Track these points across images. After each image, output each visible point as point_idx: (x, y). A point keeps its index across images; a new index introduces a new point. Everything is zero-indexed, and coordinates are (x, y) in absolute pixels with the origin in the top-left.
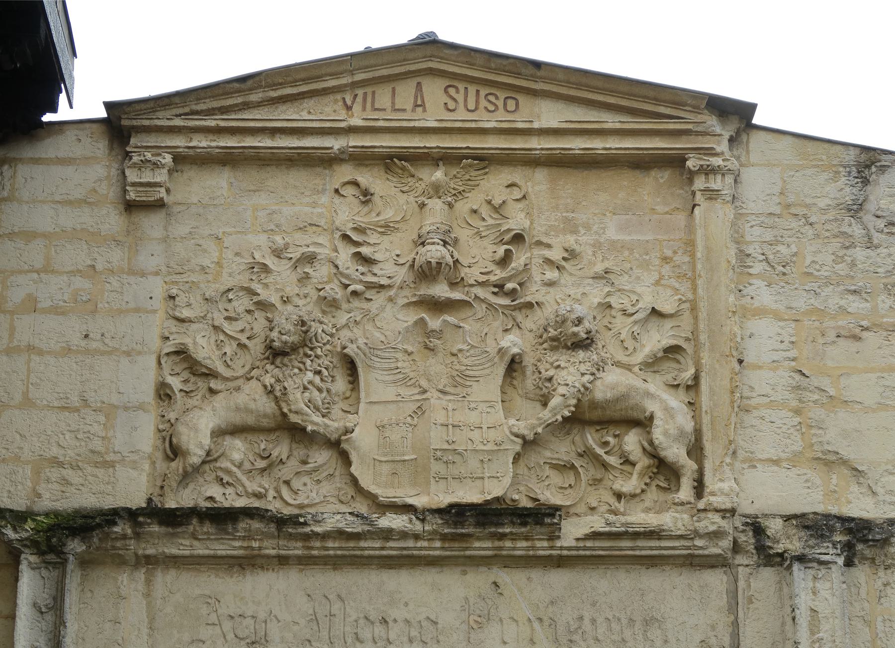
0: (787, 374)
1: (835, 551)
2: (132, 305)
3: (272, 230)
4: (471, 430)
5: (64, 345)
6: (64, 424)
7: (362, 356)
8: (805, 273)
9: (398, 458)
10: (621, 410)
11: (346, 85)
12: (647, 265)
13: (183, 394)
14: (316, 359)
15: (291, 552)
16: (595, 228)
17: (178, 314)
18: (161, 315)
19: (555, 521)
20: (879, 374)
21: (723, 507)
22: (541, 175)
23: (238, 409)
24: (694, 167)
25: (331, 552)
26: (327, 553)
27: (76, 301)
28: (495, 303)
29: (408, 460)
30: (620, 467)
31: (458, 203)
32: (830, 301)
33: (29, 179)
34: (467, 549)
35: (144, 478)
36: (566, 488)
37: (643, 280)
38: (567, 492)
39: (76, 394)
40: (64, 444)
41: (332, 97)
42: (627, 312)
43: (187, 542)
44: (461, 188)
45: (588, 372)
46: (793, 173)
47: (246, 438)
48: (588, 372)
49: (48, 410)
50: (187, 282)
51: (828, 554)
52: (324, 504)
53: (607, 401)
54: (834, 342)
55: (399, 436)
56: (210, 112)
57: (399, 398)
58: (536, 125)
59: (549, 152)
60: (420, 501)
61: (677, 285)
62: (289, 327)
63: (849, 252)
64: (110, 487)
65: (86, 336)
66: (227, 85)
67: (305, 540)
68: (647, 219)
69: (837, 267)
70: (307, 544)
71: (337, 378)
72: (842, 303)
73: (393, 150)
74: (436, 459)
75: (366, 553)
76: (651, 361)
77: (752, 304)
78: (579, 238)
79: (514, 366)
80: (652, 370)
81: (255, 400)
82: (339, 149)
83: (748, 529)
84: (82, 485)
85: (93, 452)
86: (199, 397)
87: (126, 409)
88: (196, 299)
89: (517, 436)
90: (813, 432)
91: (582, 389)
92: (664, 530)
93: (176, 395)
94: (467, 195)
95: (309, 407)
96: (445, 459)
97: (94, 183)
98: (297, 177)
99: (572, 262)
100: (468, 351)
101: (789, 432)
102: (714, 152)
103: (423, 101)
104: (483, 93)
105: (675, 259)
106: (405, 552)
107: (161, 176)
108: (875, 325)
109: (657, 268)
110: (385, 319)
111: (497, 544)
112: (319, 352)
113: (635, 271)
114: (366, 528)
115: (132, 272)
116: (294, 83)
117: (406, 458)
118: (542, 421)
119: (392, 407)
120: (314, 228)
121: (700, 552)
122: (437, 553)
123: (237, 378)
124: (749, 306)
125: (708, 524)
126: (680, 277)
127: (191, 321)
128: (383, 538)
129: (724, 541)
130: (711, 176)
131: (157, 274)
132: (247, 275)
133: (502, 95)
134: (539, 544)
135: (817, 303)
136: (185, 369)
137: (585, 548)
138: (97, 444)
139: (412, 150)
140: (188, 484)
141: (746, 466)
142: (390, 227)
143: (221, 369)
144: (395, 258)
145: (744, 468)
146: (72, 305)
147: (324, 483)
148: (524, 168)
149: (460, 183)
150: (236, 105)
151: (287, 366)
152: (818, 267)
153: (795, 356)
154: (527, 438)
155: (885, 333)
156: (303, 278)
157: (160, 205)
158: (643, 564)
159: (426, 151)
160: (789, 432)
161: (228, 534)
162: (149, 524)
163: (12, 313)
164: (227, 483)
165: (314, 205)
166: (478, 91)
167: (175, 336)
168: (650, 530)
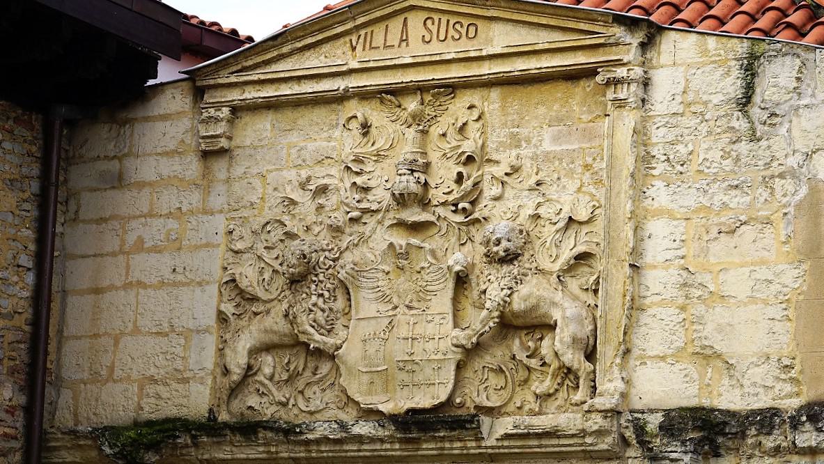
0: (677, 272)
1: (683, 449)
2: (204, 241)
3: (300, 165)
4: (427, 341)
5: (160, 279)
6: (159, 347)
7: (351, 279)
8: (698, 171)
9: (374, 369)
10: (536, 317)
11: (351, 29)
12: (572, 173)
13: (236, 316)
14: (319, 283)
15: (298, 455)
16: (534, 141)
17: (233, 247)
18: (223, 248)
19: (474, 426)
20: (752, 268)
21: (603, 408)
22: (495, 94)
23: (266, 331)
24: (603, 81)
25: (325, 454)
26: (322, 455)
27: (168, 240)
28: (453, 222)
29: (381, 371)
30: (540, 368)
31: (431, 128)
32: (715, 198)
33: (142, 135)
34: (418, 449)
35: (208, 392)
36: (500, 390)
37: (568, 189)
38: (500, 393)
39: (167, 321)
40: (158, 365)
41: (342, 40)
42: (552, 221)
43: (228, 449)
44: (434, 114)
45: (506, 287)
46: (693, 71)
47: (277, 352)
48: (506, 287)
49: (149, 336)
50: (241, 218)
51: (676, 452)
52: (327, 410)
53: (525, 312)
54: (716, 238)
55: (374, 350)
56: (256, 66)
57: (378, 315)
58: (484, 53)
59: (495, 76)
60: (386, 408)
61: (594, 191)
62: (294, 261)
63: (735, 147)
64: (185, 400)
65: (174, 270)
66: (264, 44)
67: (306, 445)
68: (575, 129)
69: (725, 163)
70: (307, 448)
71: (338, 297)
72: (725, 199)
73: (381, 87)
74: (400, 369)
75: (349, 454)
76: (566, 268)
77: (652, 206)
78: (522, 152)
79: (461, 280)
80: (570, 275)
81: (277, 323)
82: (343, 90)
83: (629, 425)
84: (169, 399)
85: (176, 370)
86: (247, 319)
87: (198, 332)
88: (246, 232)
89: (457, 346)
90: (694, 327)
91: (502, 303)
92: (558, 431)
93: (230, 318)
94: (439, 119)
95: (313, 327)
96: (407, 368)
97: (183, 134)
98: (319, 114)
99: (515, 176)
100: (429, 268)
101: (675, 328)
102: (622, 62)
103: (407, 36)
104: (451, 23)
105: (594, 166)
106: (376, 453)
107: (220, 129)
108: (752, 218)
109: (579, 176)
110: (376, 239)
111: (439, 445)
112: (321, 277)
113: (563, 180)
114: (344, 435)
115: (205, 212)
116: (312, 34)
117: (379, 369)
118: (475, 332)
119: (373, 322)
120: (329, 160)
121: (591, 448)
122: (398, 453)
123: (272, 300)
124: (650, 207)
125: (592, 424)
126: (598, 182)
127: (242, 252)
128: (358, 442)
129: (608, 438)
130: (619, 86)
131: (221, 212)
132: (281, 208)
133: (466, 22)
134: (469, 444)
135: (705, 201)
136: (237, 295)
137: (503, 447)
138: (179, 364)
139: (394, 86)
140: (237, 395)
141: (638, 363)
142: (380, 155)
143: (261, 293)
144: (384, 183)
145: (636, 366)
146: (166, 243)
147: (327, 391)
148: (482, 89)
149: (433, 110)
150: (274, 57)
151: (299, 291)
152: (708, 164)
153: (684, 254)
154: (466, 347)
155: (760, 226)
156: (318, 208)
157: (223, 152)
158: (556, 458)
159: (404, 85)
160: (675, 328)
161: (253, 441)
162: (201, 436)
163: (128, 253)
164: (263, 393)
165: (329, 139)
166: (448, 21)
167: (231, 266)
168: (547, 432)
